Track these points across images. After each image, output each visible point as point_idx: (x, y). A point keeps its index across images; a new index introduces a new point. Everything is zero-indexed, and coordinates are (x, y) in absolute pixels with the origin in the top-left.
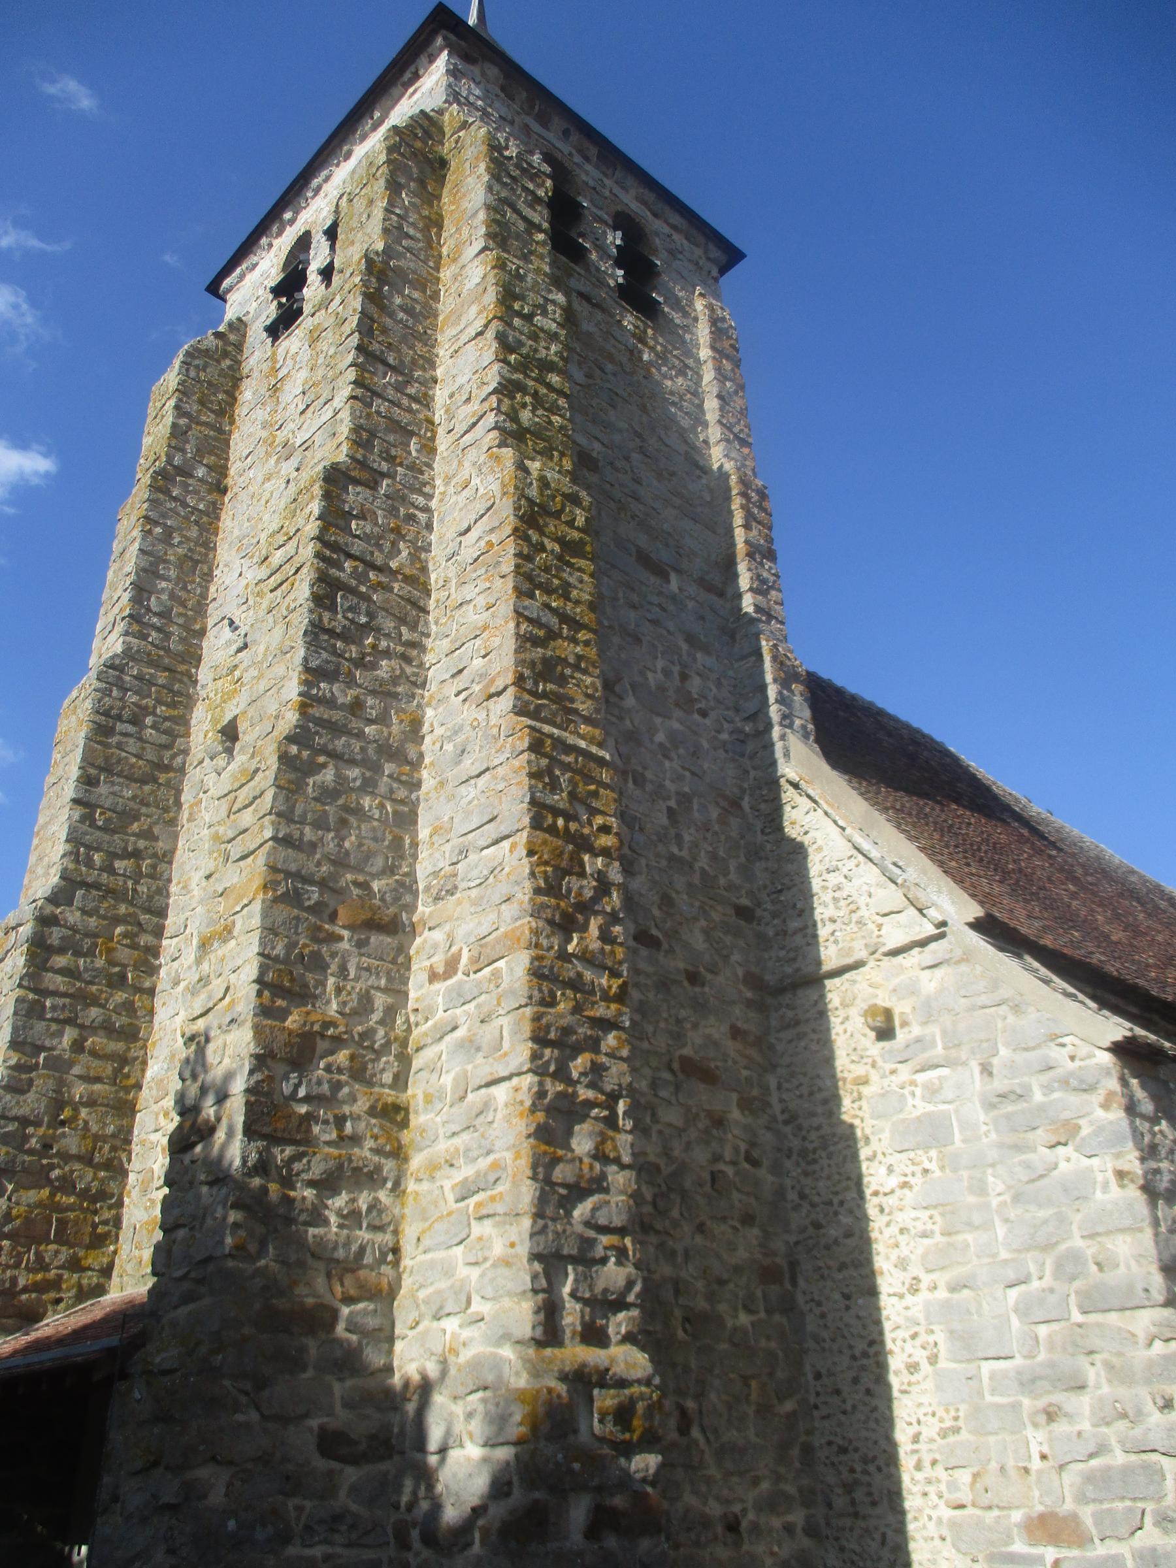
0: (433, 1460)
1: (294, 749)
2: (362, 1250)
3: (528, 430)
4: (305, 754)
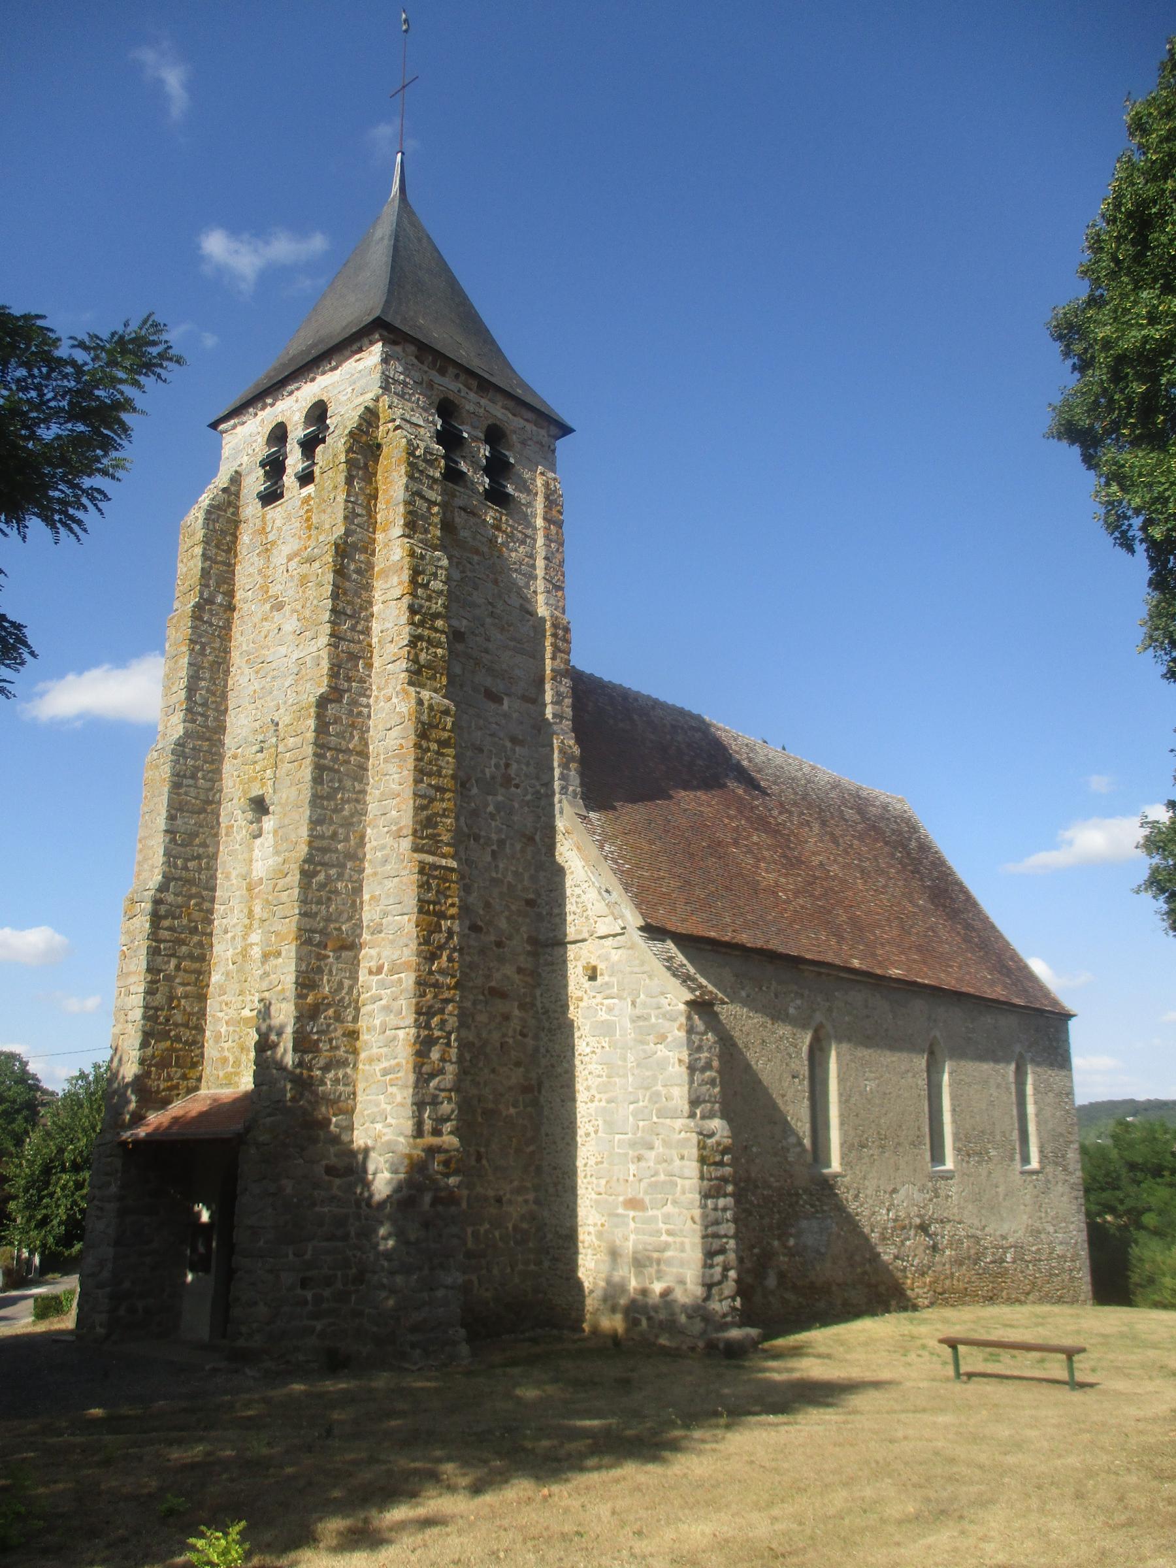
0: (370, 1177)
1: (306, 866)
2: (341, 1094)
3: (423, 666)
4: (312, 867)
